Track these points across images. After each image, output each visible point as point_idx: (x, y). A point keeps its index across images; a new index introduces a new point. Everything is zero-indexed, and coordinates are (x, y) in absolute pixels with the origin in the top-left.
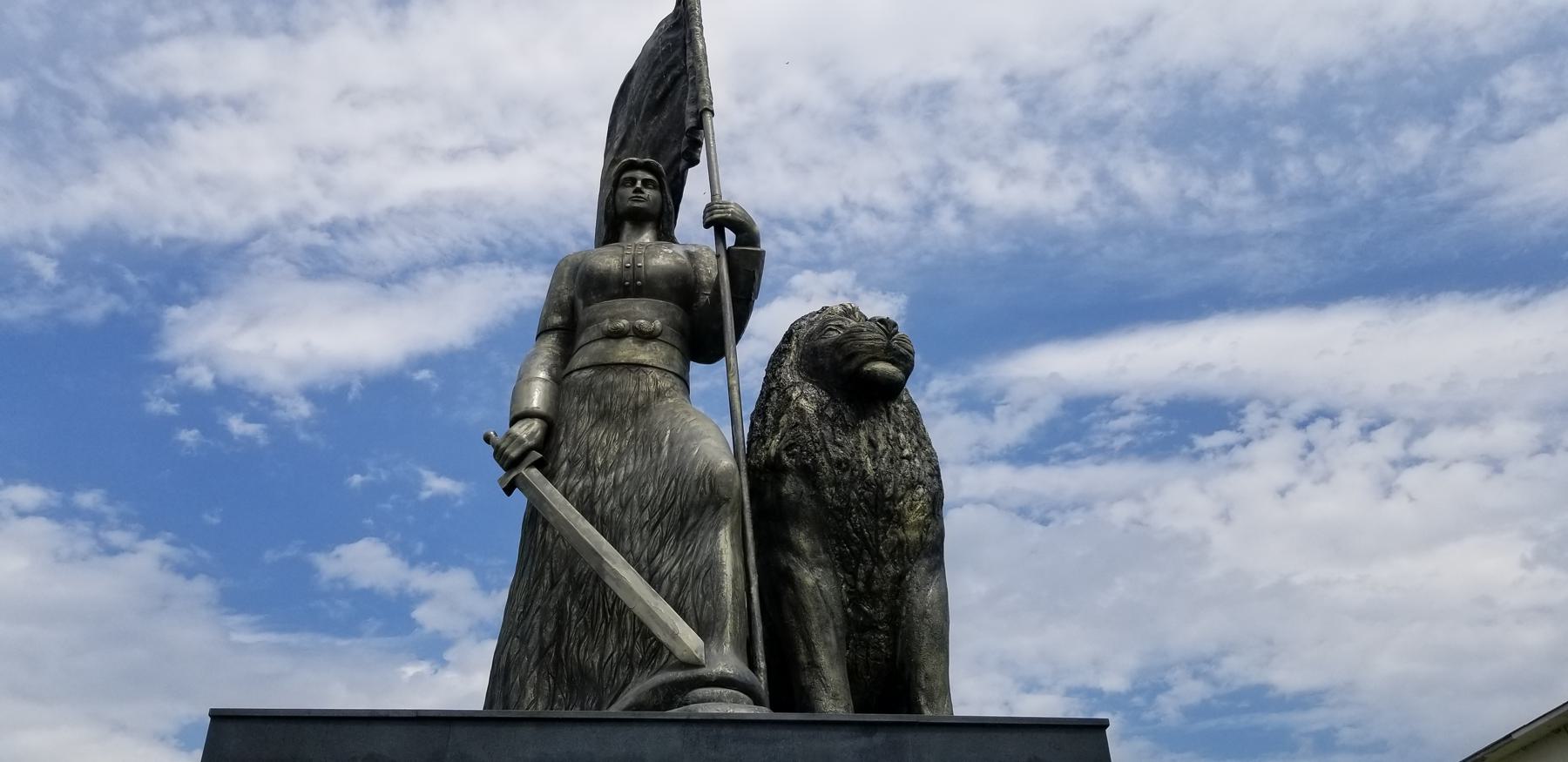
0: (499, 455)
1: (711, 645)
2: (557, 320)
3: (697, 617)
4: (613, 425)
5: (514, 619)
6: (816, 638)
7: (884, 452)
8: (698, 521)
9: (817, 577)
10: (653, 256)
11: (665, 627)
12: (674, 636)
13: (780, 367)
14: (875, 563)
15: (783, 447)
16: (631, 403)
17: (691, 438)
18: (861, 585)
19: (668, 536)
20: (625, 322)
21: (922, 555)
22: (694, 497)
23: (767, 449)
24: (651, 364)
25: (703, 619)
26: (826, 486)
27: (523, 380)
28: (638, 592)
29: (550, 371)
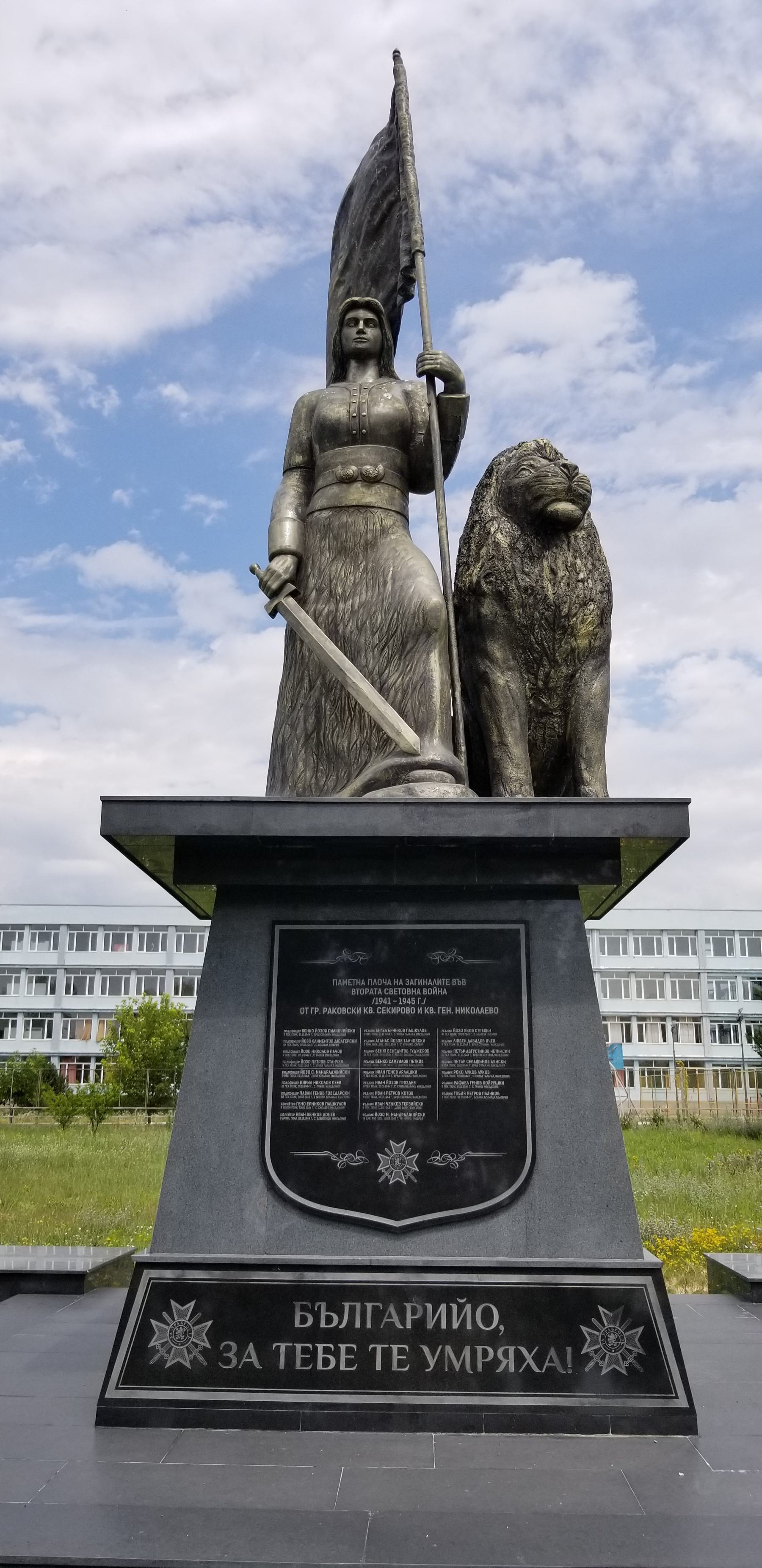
0: (263, 585)
1: (425, 739)
2: (299, 459)
3: (414, 718)
4: (349, 559)
5: (285, 710)
6: (505, 724)
7: (562, 577)
8: (415, 646)
9: (507, 679)
10: (375, 404)
11: (392, 727)
12: (399, 733)
13: (483, 501)
14: (552, 667)
15: (483, 575)
16: (362, 540)
17: (409, 576)
18: (540, 683)
19: (393, 656)
20: (354, 468)
21: (590, 657)
22: (411, 627)
23: (471, 575)
24: (376, 505)
25: (420, 720)
26: (515, 608)
27: (275, 518)
28: (372, 700)
29: (296, 510)
